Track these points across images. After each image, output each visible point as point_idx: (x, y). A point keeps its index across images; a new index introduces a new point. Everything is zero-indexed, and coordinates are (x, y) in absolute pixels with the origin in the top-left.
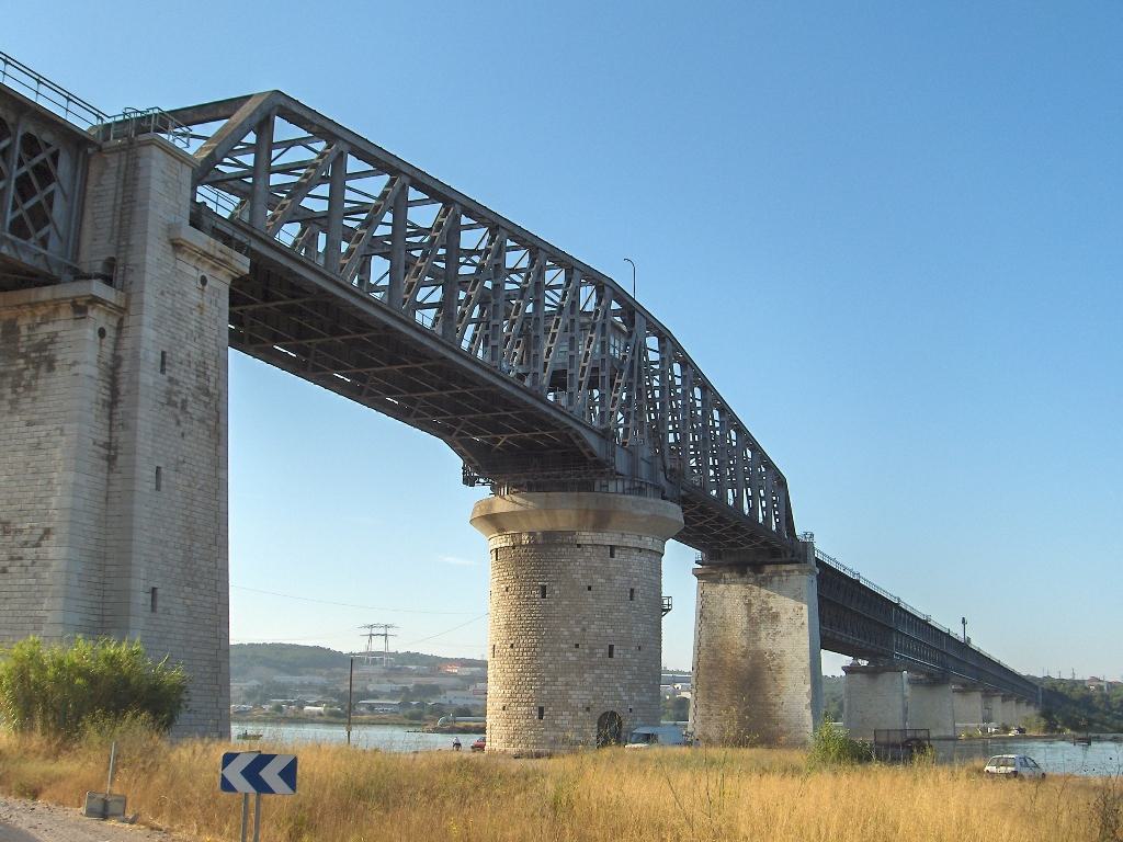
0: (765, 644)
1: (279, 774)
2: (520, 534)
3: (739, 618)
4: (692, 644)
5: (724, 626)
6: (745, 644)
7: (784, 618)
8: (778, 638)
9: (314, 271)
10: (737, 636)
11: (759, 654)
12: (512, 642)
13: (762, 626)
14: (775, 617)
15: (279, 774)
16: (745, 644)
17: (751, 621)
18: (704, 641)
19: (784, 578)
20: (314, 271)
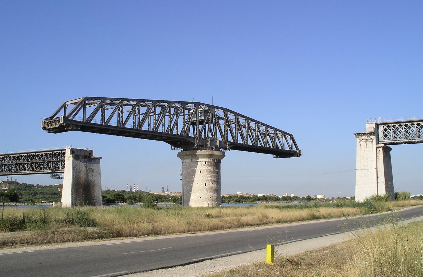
0: (91, 178)
1: (92, 151)
2: (215, 159)
3: (84, 170)
4: (71, 177)
5: (80, 172)
6: (85, 178)
7: (95, 171)
8: (93, 176)
9: (112, 244)
10: (83, 175)
11: (89, 181)
12: (213, 183)
13: (90, 173)
14: (93, 171)
15: (92, 151)
16: (85, 178)
17: (87, 171)
18: (74, 176)
19: (95, 160)
20: (112, 244)
